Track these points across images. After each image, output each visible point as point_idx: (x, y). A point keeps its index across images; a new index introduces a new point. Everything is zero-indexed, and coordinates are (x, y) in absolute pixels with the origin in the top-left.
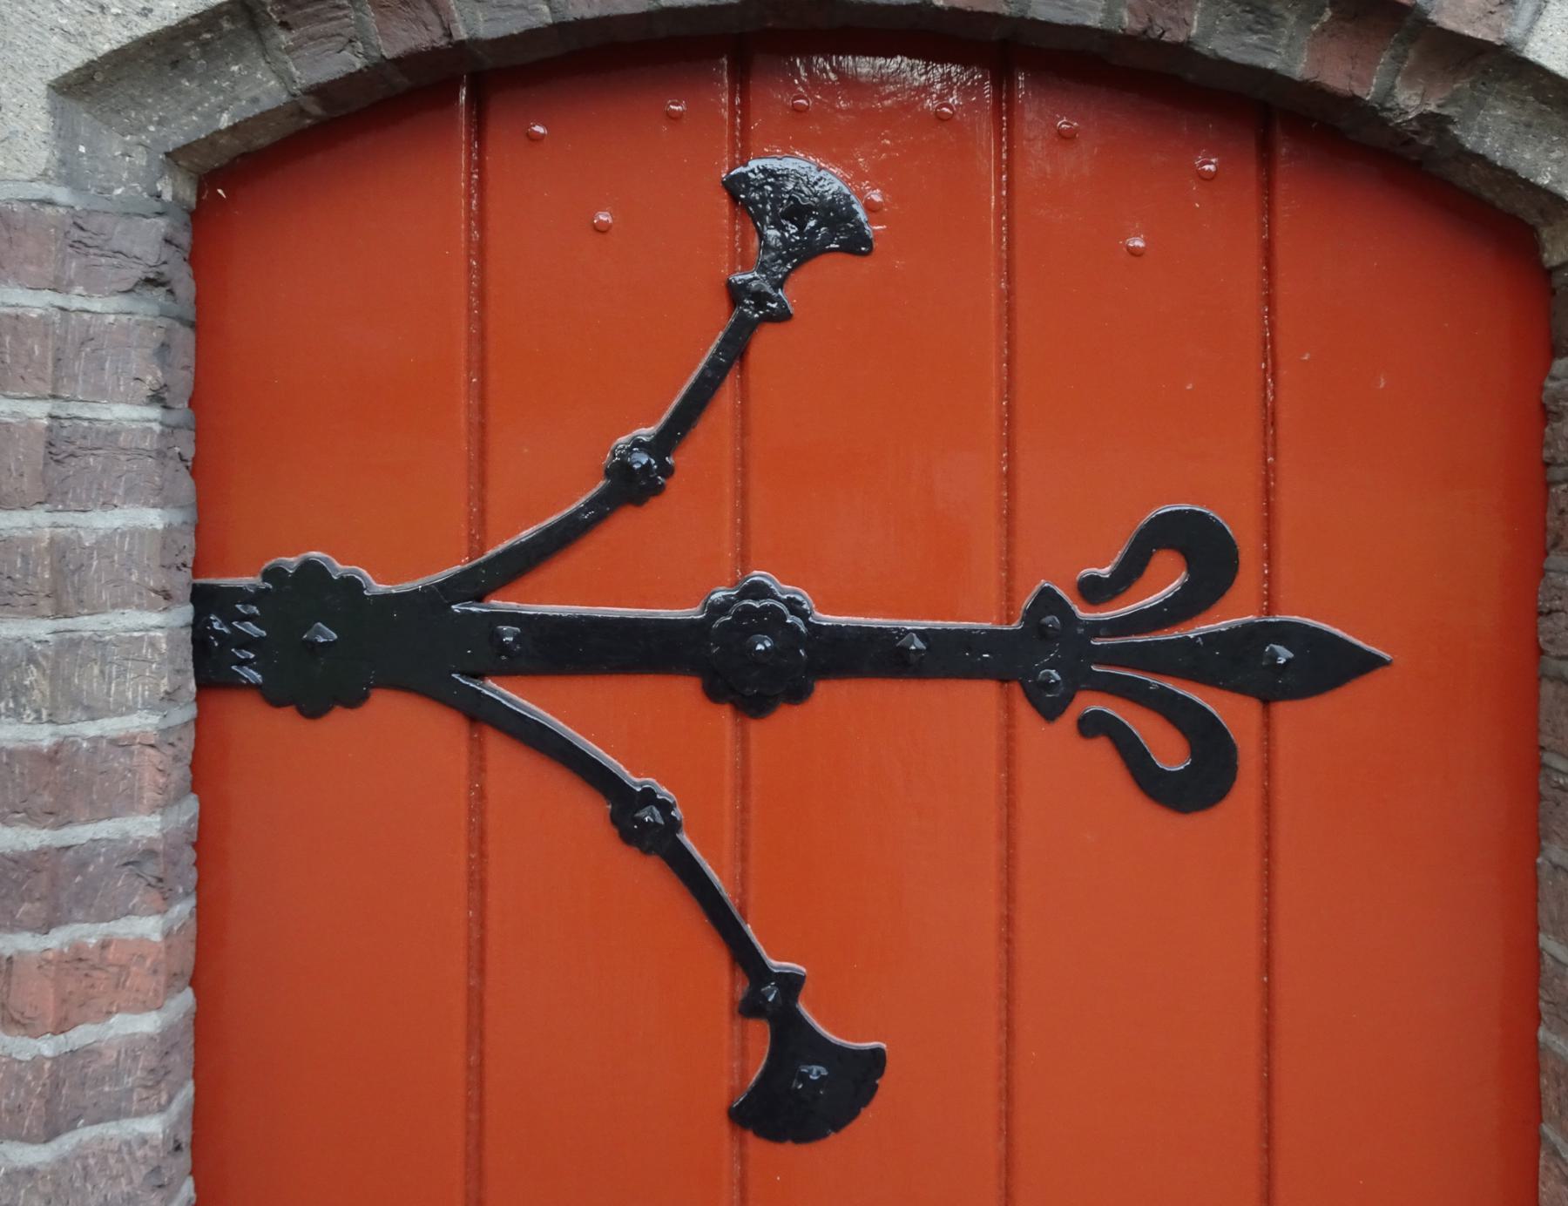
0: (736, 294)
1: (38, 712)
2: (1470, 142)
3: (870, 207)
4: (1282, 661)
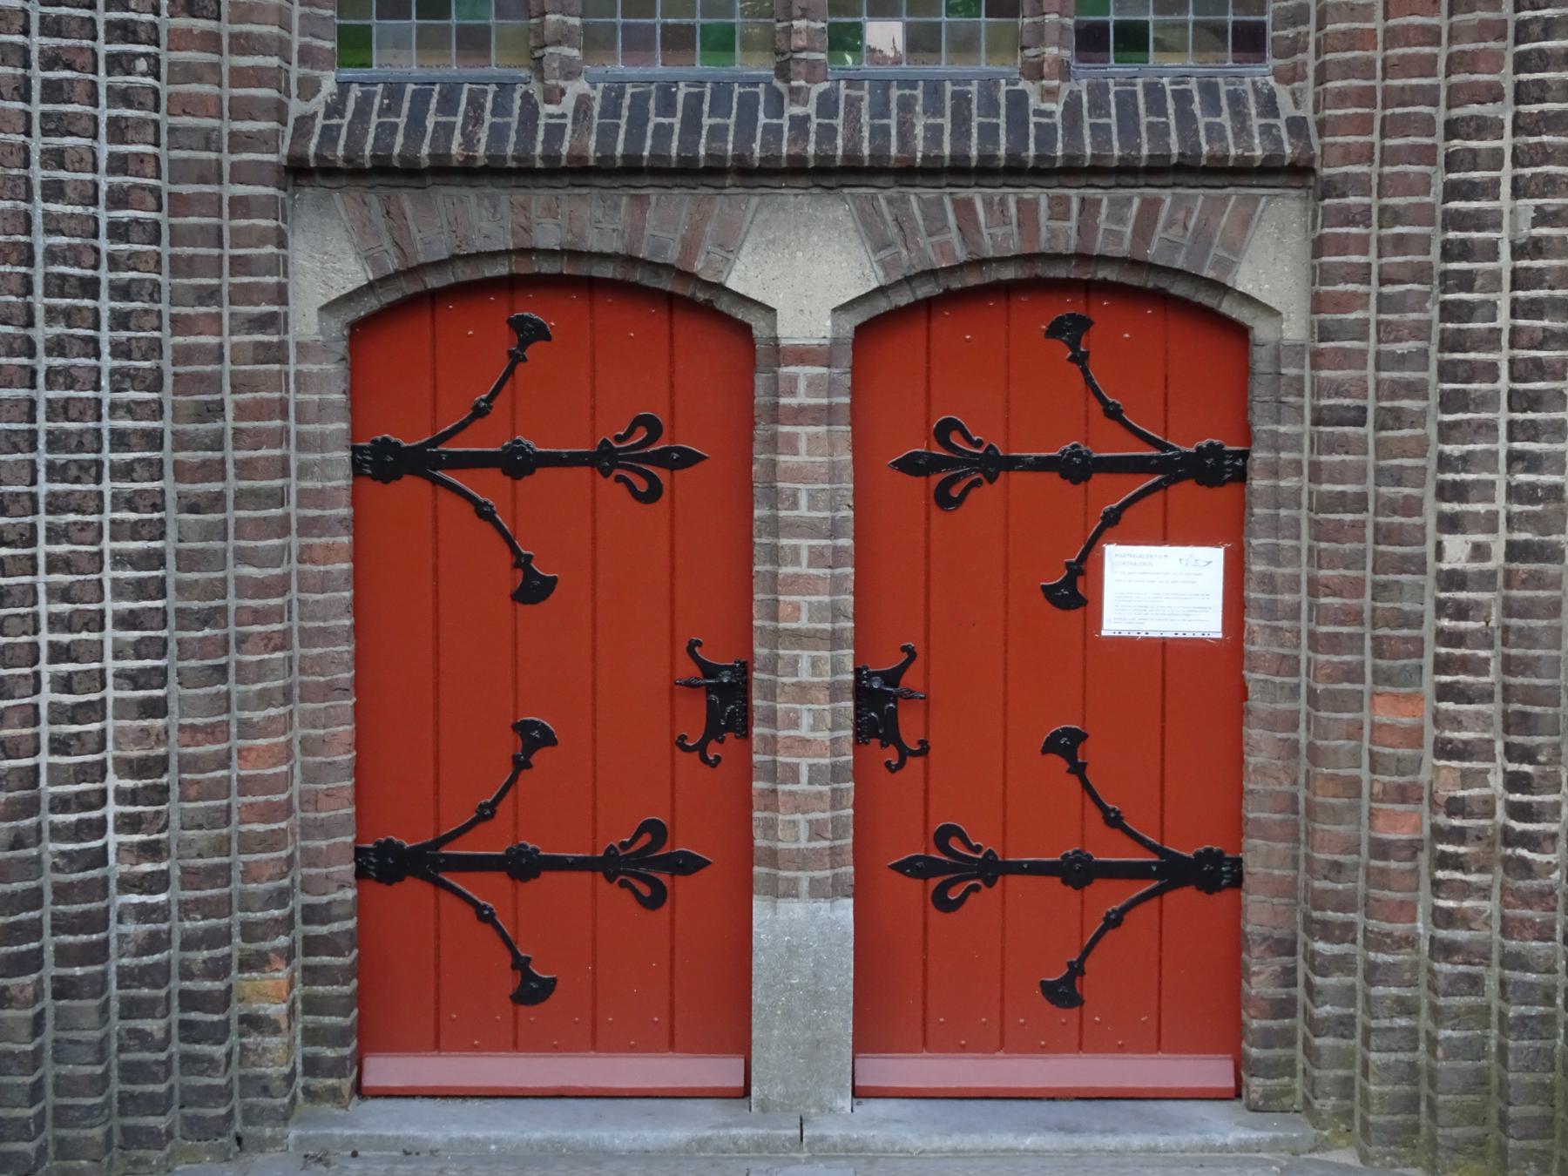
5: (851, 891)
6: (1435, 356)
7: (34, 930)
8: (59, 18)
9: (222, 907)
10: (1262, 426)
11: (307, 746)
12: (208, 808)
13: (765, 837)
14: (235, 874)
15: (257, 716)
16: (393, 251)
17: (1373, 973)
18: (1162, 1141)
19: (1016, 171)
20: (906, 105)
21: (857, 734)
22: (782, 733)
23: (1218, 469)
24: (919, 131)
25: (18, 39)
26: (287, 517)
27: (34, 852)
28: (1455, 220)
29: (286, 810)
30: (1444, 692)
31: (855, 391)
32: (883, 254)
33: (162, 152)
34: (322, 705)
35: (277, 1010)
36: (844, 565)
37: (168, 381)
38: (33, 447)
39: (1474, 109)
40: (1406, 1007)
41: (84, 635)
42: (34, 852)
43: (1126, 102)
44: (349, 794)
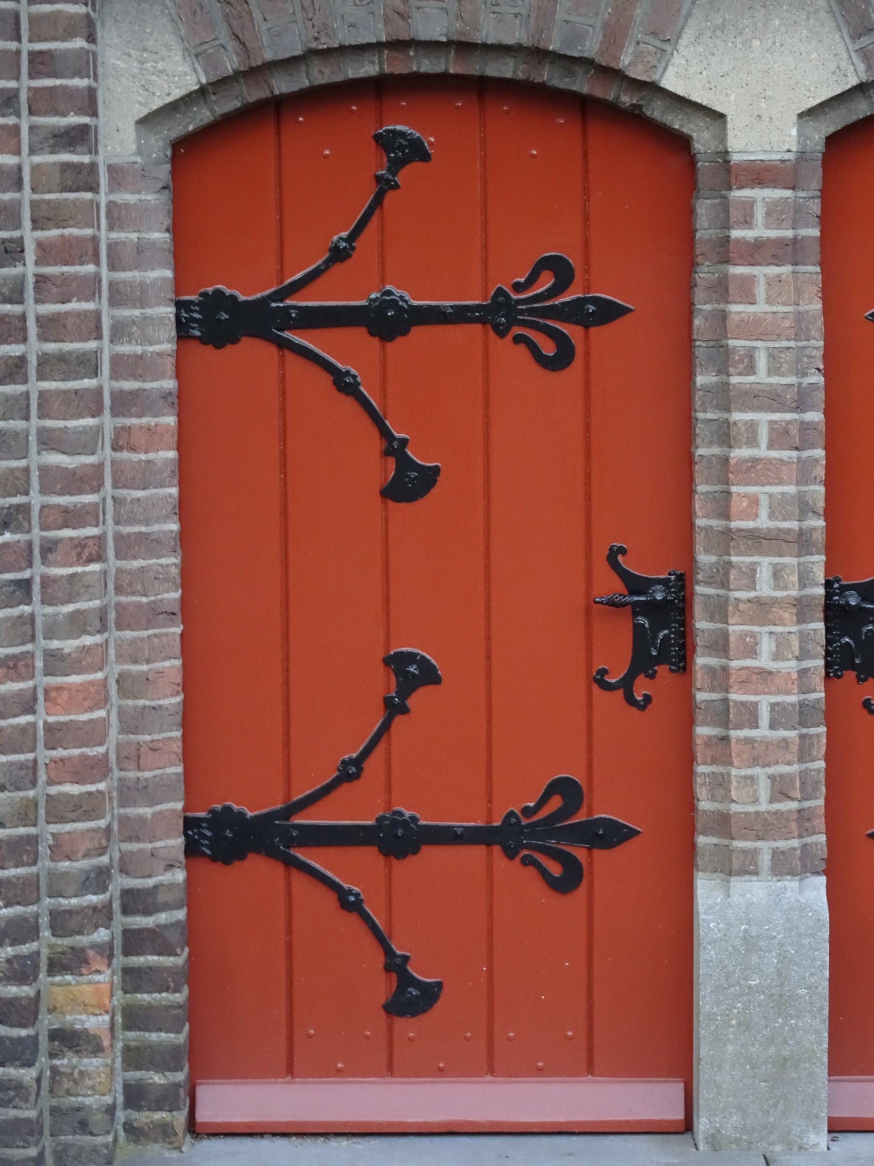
0: (378, 179)
1: (137, 341)
2: (649, 113)
3: (430, 143)
4: (591, 311)
5: (823, 866)
12: (11, 764)
13: (713, 798)
14: (43, 849)
15: (69, 645)
16: (231, 45)
21: (828, 665)
22: (735, 664)
26: (99, 391)
31: (824, 220)
32: (865, 41)
34: (145, 633)
36: (812, 446)
44: (177, 747)
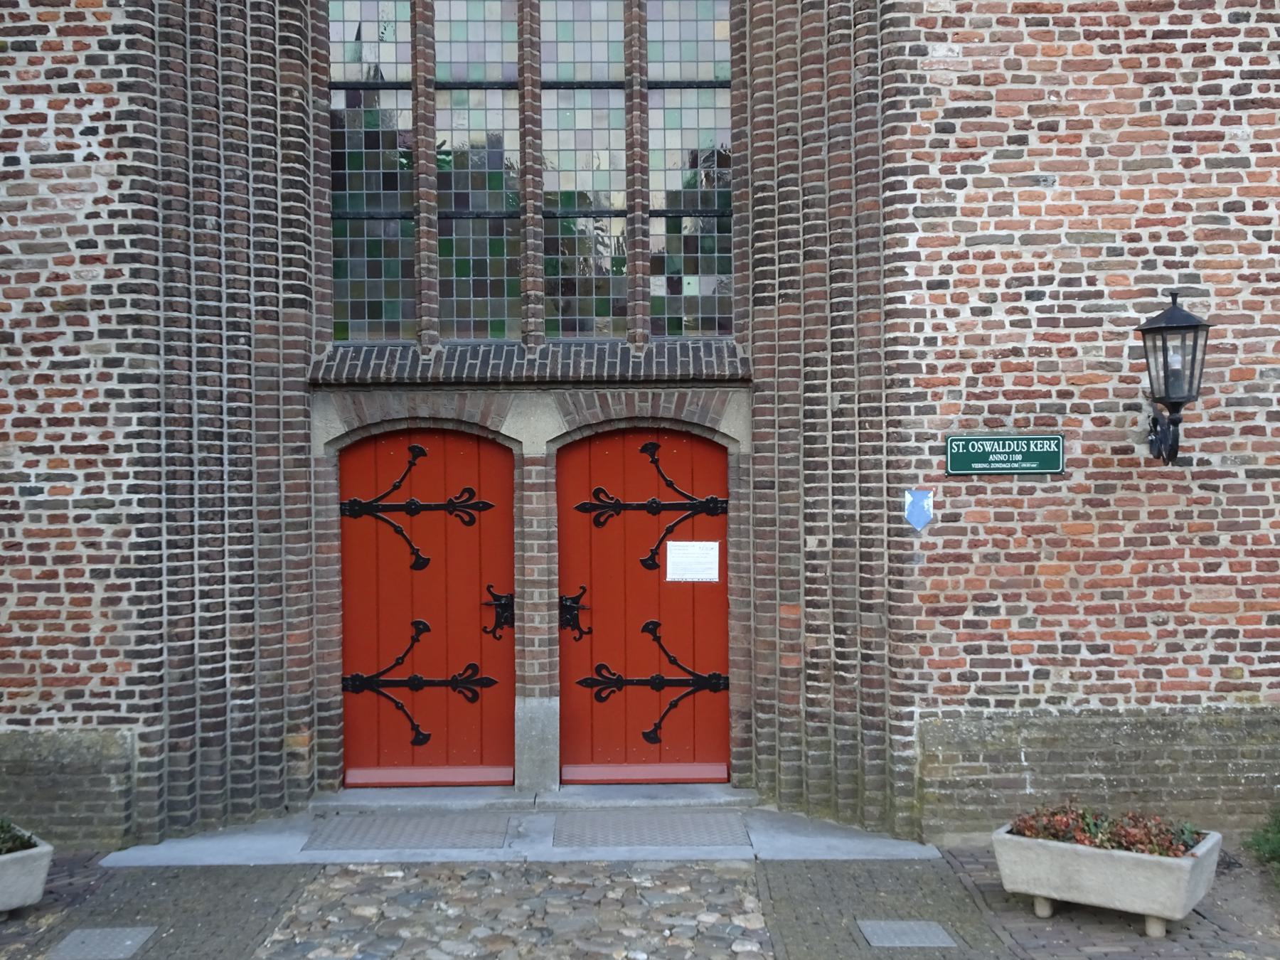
6: (802, 459)
7: (191, 717)
8: (204, 321)
9: (280, 704)
10: (733, 490)
11: (320, 633)
14: (285, 690)
15: (295, 620)
17: (782, 726)
18: (692, 802)
19: (624, 382)
20: (578, 354)
23: (716, 508)
24: (583, 365)
25: (186, 330)
27: (191, 682)
28: (809, 401)
29: (310, 661)
30: (809, 604)
31: (558, 476)
33: (252, 378)
35: (303, 750)
37: (255, 476)
38: (192, 506)
39: (815, 354)
40: (796, 742)
41: (215, 587)
42: (191, 682)
43: (672, 352)
44: (339, 654)
